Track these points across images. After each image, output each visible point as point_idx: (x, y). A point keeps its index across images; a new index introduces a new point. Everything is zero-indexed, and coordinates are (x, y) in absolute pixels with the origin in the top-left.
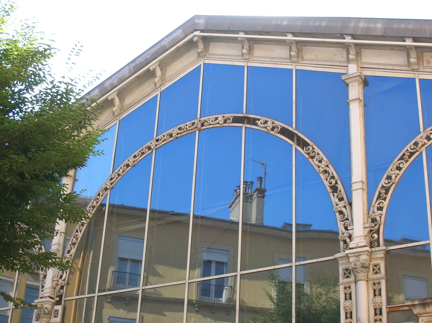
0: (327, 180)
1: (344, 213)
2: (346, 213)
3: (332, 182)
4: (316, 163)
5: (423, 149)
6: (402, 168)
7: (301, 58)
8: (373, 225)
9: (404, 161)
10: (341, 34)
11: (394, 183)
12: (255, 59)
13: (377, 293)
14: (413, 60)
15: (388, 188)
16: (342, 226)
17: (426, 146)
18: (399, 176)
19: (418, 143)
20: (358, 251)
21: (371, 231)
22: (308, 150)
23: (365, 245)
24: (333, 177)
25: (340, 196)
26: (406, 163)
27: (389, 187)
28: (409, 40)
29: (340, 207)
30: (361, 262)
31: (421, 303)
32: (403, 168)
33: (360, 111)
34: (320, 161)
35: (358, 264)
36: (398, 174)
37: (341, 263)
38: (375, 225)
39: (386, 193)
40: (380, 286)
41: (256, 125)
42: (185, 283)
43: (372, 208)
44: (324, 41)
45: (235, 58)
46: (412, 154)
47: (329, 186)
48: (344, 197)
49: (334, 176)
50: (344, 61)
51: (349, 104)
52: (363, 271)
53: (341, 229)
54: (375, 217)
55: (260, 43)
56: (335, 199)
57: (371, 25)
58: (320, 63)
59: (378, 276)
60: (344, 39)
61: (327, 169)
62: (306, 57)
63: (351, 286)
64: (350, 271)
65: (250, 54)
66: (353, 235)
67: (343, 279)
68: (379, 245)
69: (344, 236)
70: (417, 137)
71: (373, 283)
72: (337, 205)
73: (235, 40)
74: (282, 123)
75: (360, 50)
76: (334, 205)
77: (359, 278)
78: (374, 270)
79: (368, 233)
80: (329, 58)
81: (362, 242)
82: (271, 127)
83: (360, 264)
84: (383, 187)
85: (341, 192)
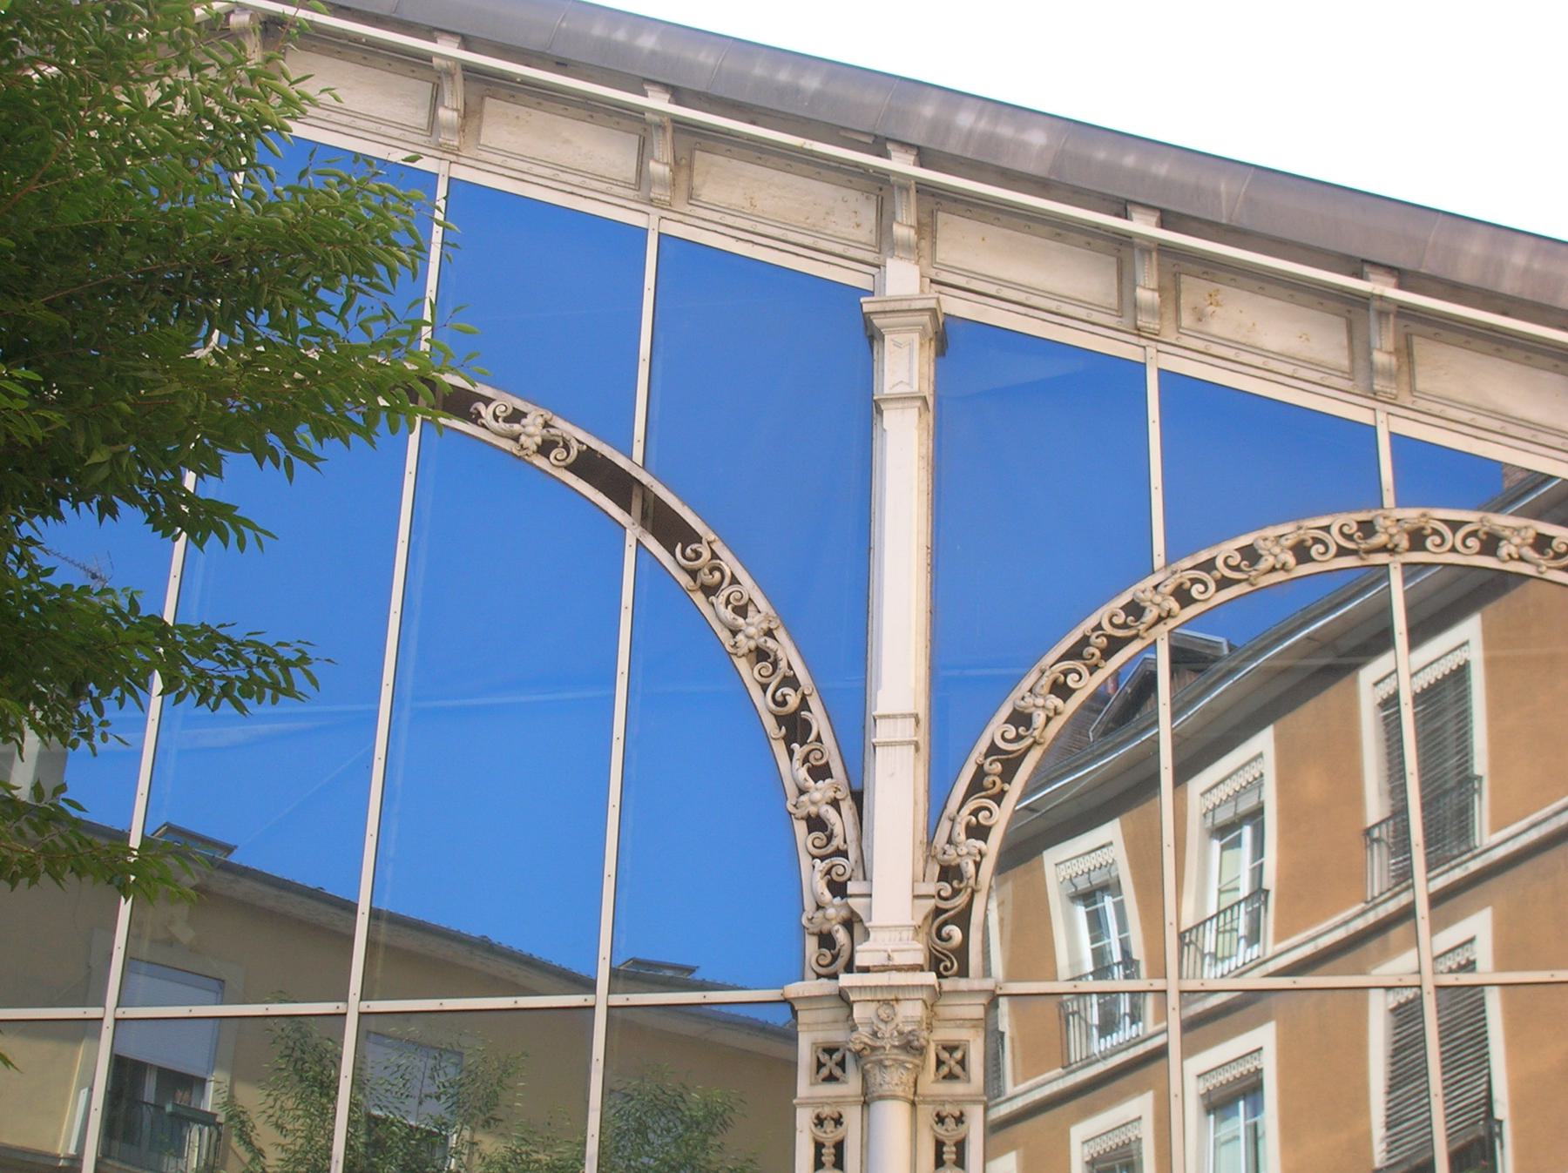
0: (764, 688)
1: (830, 826)
2: (838, 830)
3: (788, 697)
7: (684, 195)
8: (947, 890)
9: (1085, 665)
10: (876, 136)
11: (1039, 744)
12: (485, 156)
14: (447, 115)
15: (1017, 757)
16: (818, 876)
17: (1172, 623)
18: (1058, 717)
20: (892, 983)
21: (938, 912)
22: (693, 555)
24: (791, 681)
25: (817, 760)
26: (1091, 674)
28: (1149, 218)
29: (814, 803)
33: (920, 444)
34: (741, 611)
36: (1057, 712)
37: (807, 1021)
38: (956, 893)
39: (1008, 774)
40: (962, 1128)
41: (475, 422)
42: (102, 1019)
43: (945, 826)
45: (396, 133)
46: (1114, 646)
47: (771, 712)
48: (832, 765)
49: (795, 674)
50: (865, 244)
51: (880, 412)
52: (904, 1062)
54: (958, 860)
55: (511, 100)
56: (797, 766)
57: (1006, 131)
58: (760, 228)
59: (958, 1088)
60: (886, 155)
61: (771, 643)
62: (707, 193)
63: (844, 1115)
64: (844, 1057)
65: (464, 131)
67: (812, 1084)
68: (963, 972)
70: (1140, 586)
72: (802, 792)
73: (421, 61)
74: (588, 431)
76: (791, 790)
77: (886, 1087)
78: (940, 1063)
79: (926, 918)
80: (803, 220)
81: (908, 950)
82: (539, 440)
83: (896, 1034)
84: (993, 749)
85: (821, 742)
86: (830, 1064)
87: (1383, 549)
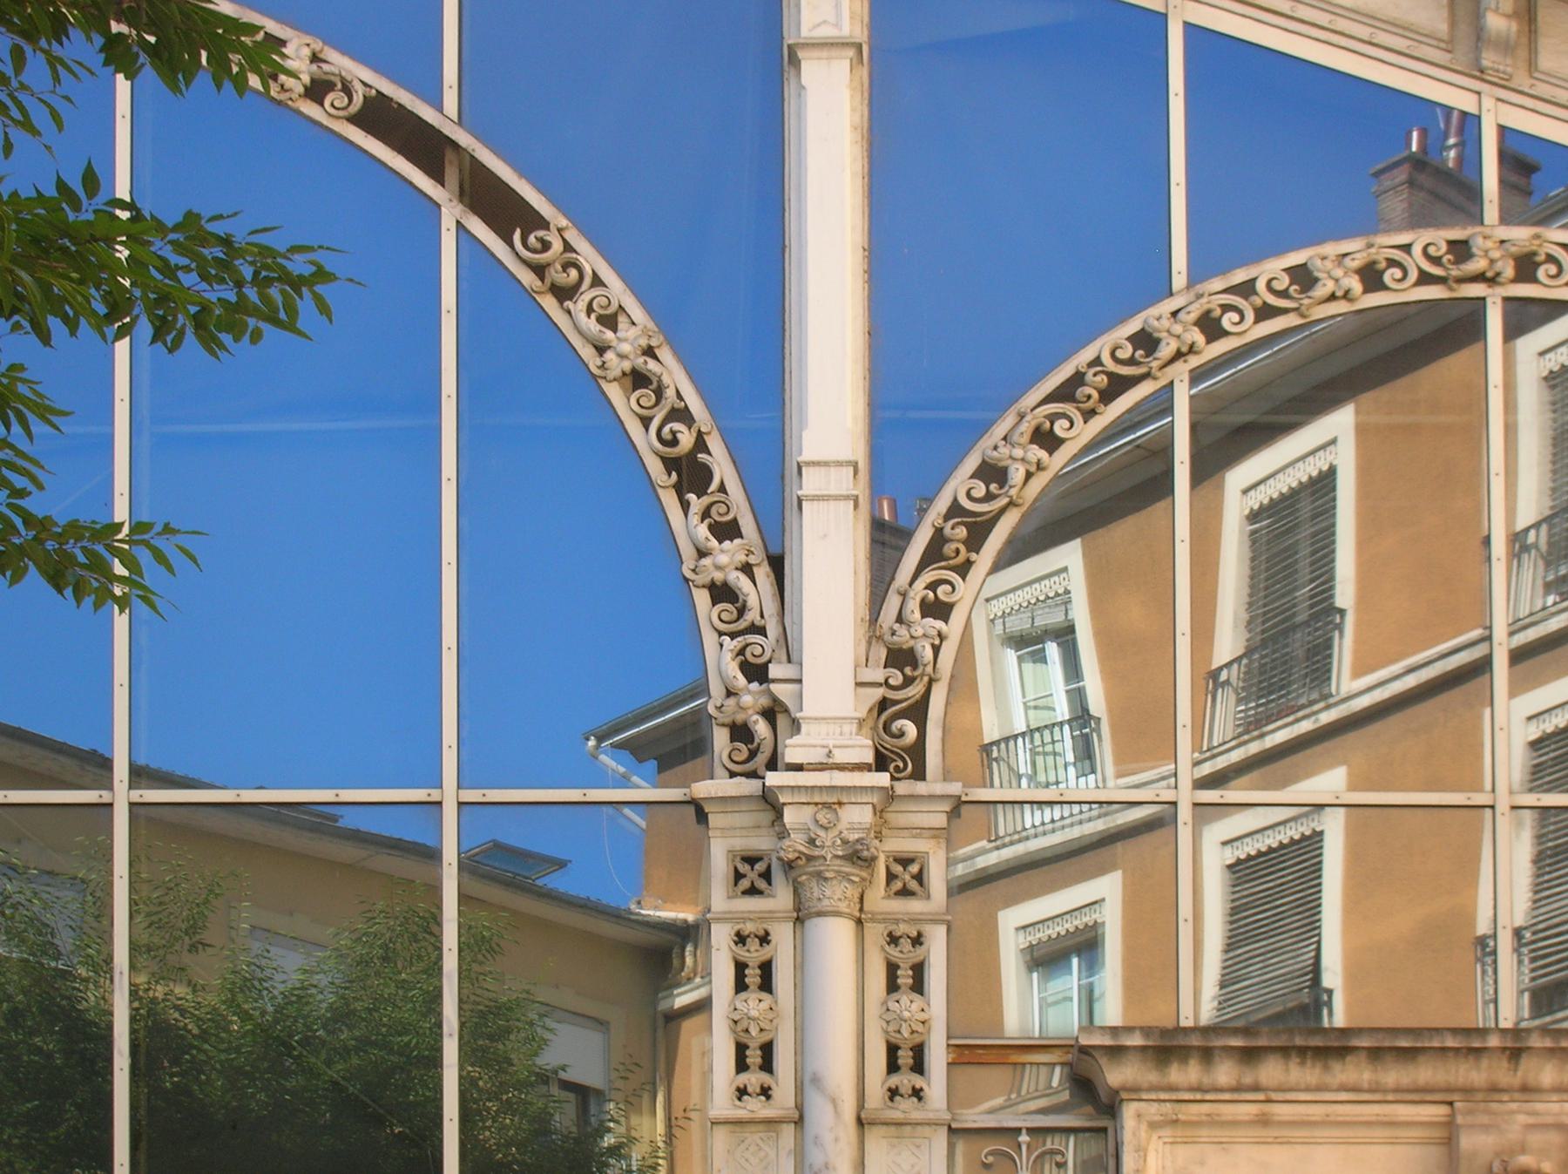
0: (646, 422)
1: (741, 597)
2: (752, 601)
3: (679, 436)
5: (1181, 371)
8: (897, 678)
11: (1017, 506)
15: (982, 522)
17: (1194, 361)
20: (833, 784)
21: (883, 704)
22: (539, 246)
24: (682, 414)
27: (991, 514)
29: (719, 568)
30: (845, 834)
31: (1158, 1044)
32: (1068, 443)
33: (853, 110)
34: (609, 321)
35: (828, 843)
36: (1040, 467)
38: (908, 681)
46: (1117, 386)
49: (686, 406)
52: (848, 874)
54: (912, 643)
59: (914, 906)
61: (652, 365)
63: (772, 933)
67: (729, 898)
68: (919, 774)
69: (738, 704)
70: (1153, 311)
71: (733, 933)
72: (702, 553)
74: (376, 68)
76: (687, 552)
77: (826, 902)
78: (891, 877)
83: (839, 842)
84: (955, 510)
85: (727, 494)
86: (752, 875)
87: (1479, 278)
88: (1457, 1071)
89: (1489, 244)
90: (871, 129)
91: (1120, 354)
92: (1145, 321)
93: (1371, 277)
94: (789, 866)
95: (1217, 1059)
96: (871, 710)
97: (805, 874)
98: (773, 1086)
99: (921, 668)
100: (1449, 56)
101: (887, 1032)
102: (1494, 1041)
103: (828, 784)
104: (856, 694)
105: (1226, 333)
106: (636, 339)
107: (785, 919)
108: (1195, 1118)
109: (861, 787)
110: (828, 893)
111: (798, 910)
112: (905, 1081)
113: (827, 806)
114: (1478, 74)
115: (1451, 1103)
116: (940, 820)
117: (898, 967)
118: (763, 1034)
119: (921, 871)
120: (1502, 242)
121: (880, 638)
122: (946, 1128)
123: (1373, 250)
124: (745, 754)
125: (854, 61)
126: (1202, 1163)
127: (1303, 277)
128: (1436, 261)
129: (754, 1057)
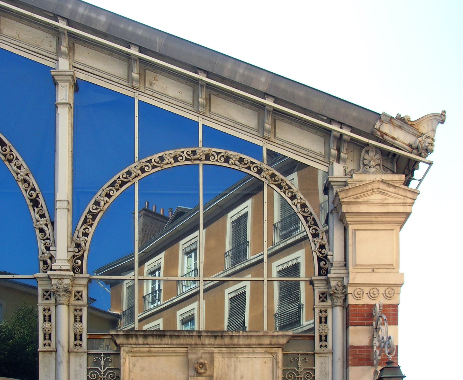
0: (26, 191)
1: (45, 231)
2: (47, 232)
3: (33, 194)
4: (14, 169)
5: (136, 180)
6: (112, 196)
9: (115, 188)
10: (54, 14)
11: (102, 211)
13: (78, 319)
15: (95, 214)
17: (139, 178)
18: (107, 203)
19: (132, 173)
20: (61, 274)
21: (74, 256)
22: (4, 150)
23: (69, 269)
24: (34, 189)
25: (41, 212)
27: (96, 213)
29: (41, 225)
34: (19, 168)
35: (61, 288)
36: (107, 202)
38: (79, 251)
43: (77, 232)
44: (33, 16)
46: (123, 183)
49: (35, 188)
51: (57, 108)
52: (65, 295)
53: (41, 249)
54: (80, 242)
57: (93, 15)
58: (22, 45)
59: (80, 302)
60: (58, 21)
61: (27, 178)
64: (50, 293)
66: (56, 257)
67: (42, 300)
68: (82, 272)
69: (44, 256)
70: (131, 166)
71: (43, 308)
72: (38, 221)
75: (73, 44)
76: (35, 221)
77: (61, 301)
78: (75, 296)
80: (34, 43)
81: (66, 266)
83: (63, 288)
84: (89, 212)
85: (42, 207)
87: (198, 159)
88: (188, 340)
89: (200, 151)
90: (74, 124)
91: (124, 176)
92: (129, 169)
93: (176, 159)
94: (331, 295)
95: (139, 337)
96: (71, 258)
97: (57, 295)
98: (51, 343)
99: (82, 248)
100: (193, 108)
101: (74, 331)
102: (195, 334)
103: (60, 274)
104: (67, 254)
105: (146, 172)
106: (24, 172)
107: (53, 305)
108: (135, 351)
109: (67, 275)
110: (61, 299)
111: (56, 303)
112: (78, 343)
113: (60, 279)
114: (198, 112)
115: (188, 348)
116: (85, 283)
117: (46, 316)
118: (49, 331)
119: (82, 294)
120: (203, 151)
121: (73, 241)
122: (86, 353)
123: (176, 153)
124: (46, 268)
125: (70, 108)
126: (138, 361)
127: (162, 159)
128: (189, 155)
129: (47, 337)
